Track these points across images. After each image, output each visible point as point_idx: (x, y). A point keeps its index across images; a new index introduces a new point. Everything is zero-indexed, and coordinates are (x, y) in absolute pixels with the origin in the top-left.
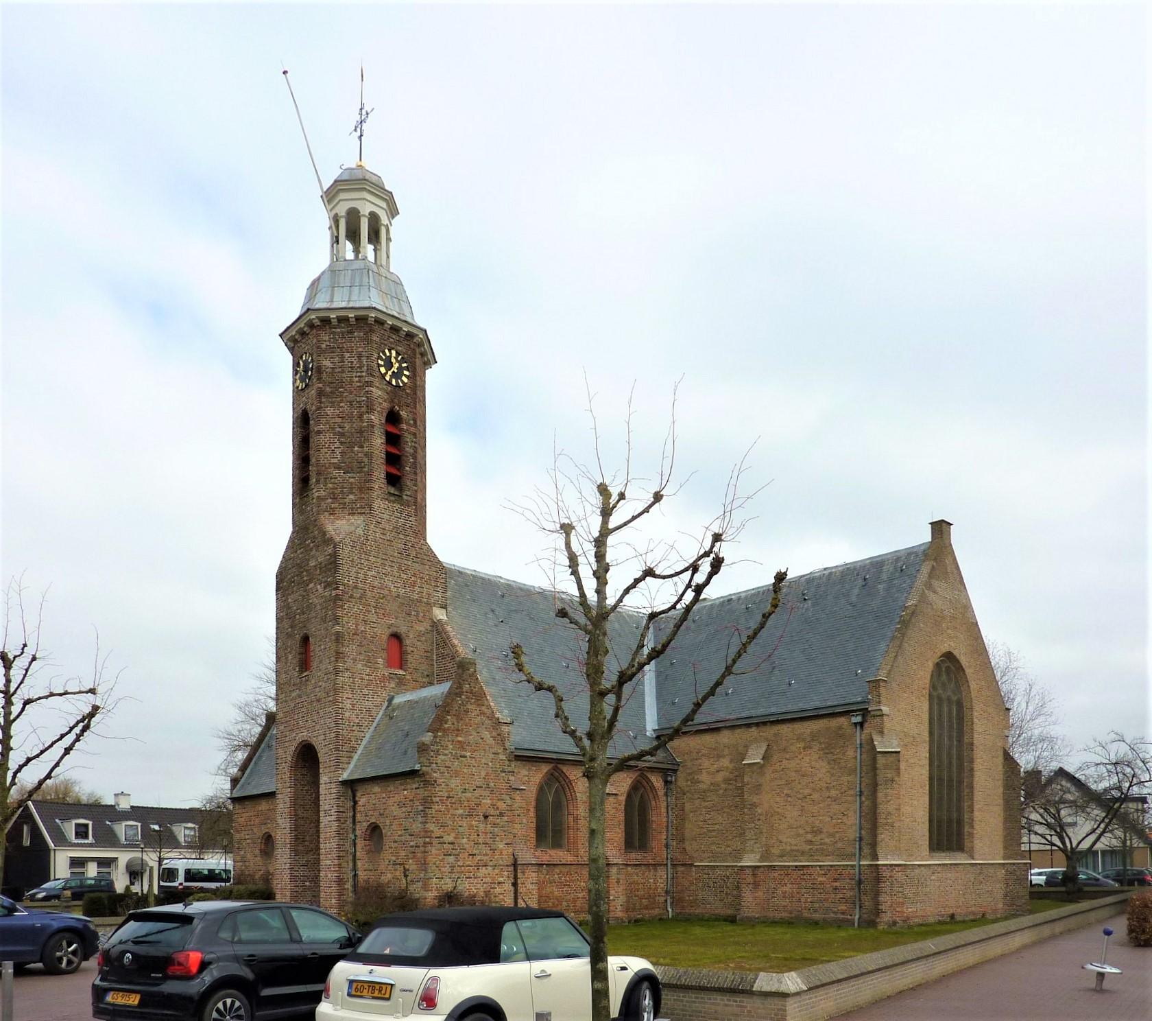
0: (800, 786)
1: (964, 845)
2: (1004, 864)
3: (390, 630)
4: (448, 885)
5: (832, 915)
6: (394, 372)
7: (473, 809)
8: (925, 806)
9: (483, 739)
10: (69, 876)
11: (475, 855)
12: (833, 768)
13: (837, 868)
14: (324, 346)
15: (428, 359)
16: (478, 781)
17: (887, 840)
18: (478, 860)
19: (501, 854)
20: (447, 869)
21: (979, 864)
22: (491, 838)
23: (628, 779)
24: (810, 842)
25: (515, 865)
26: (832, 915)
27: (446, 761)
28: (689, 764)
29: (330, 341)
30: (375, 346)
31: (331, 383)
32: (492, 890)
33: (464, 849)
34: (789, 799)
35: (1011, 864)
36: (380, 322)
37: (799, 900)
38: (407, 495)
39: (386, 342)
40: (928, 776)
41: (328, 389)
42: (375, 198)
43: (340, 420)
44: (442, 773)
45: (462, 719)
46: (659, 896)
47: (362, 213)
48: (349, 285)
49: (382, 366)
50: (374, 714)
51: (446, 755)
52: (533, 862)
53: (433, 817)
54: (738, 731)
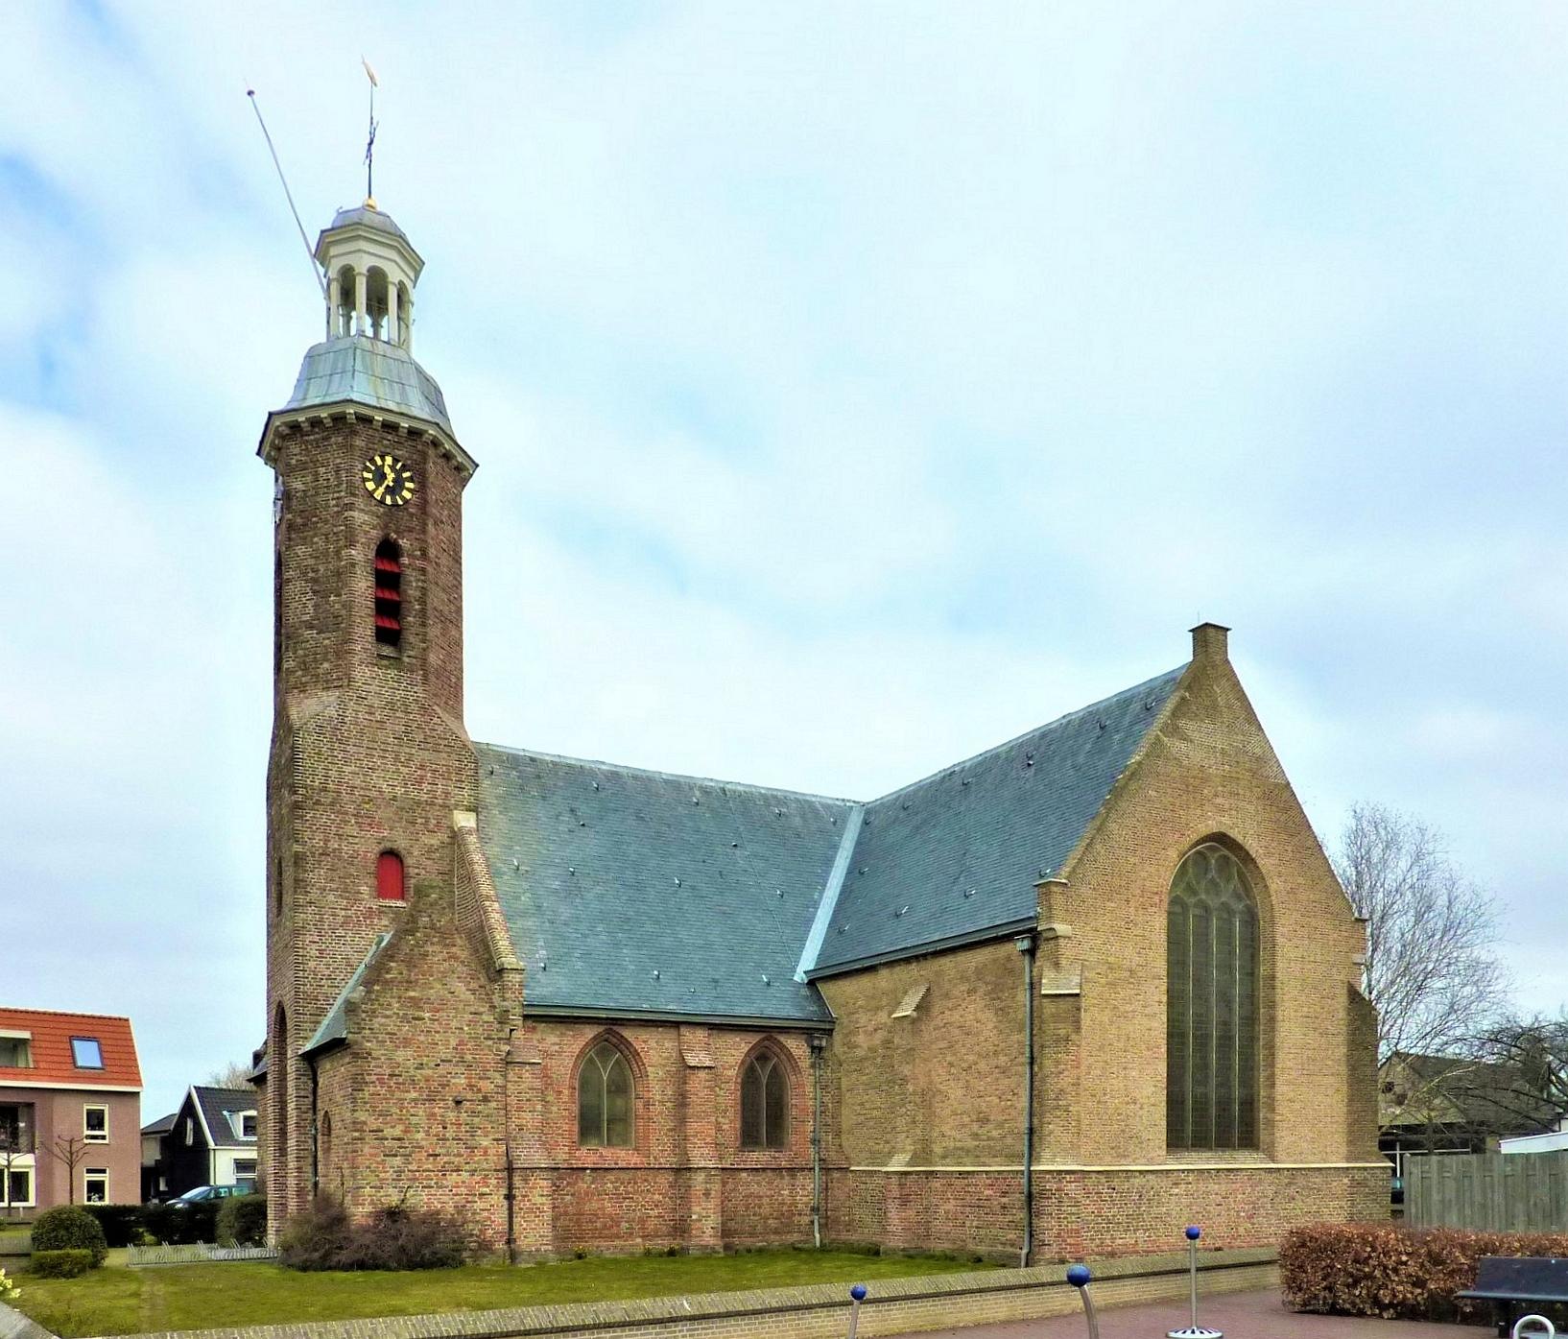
0: (964, 1051)
1: (1259, 1138)
2: (1348, 1168)
3: (382, 846)
4: (393, 1198)
5: (1000, 1248)
6: (388, 486)
7: (437, 1092)
10: (234, 1182)
12: (1000, 1022)
13: (1005, 1175)
14: (294, 462)
15: (460, 469)
16: (444, 1052)
17: (1057, 1133)
18: (445, 1163)
19: (486, 1153)
20: (390, 1174)
21: (1288, 1169)
22: (467, 1132)
23: (743, 1045)
24: (975, 1136)
25: (510, 1169)
26: (1000, 1248)
28: (845, 1021)
29: (301, 454)
30: (358, 453)
31: (302, 511)
32: (468, 1205)
33: (419, 1147)
34: (953, 1070)
35: (1359, 1168)
36: (367, 420)
37: (963, 1225)
38: (409, 657)
39: (376, 446)
40: (1165, 1031)
41: (299, 520)
43: (311, 562)
44: (381, 1041)
46: (800, 1215)
47: (357, 271)
48: (329, 372)
49: (369, 480)
50: (354, 961)
51: (387, 1017)
52: (543, 1166)
53: (365, 1103)
54: (897, 969)
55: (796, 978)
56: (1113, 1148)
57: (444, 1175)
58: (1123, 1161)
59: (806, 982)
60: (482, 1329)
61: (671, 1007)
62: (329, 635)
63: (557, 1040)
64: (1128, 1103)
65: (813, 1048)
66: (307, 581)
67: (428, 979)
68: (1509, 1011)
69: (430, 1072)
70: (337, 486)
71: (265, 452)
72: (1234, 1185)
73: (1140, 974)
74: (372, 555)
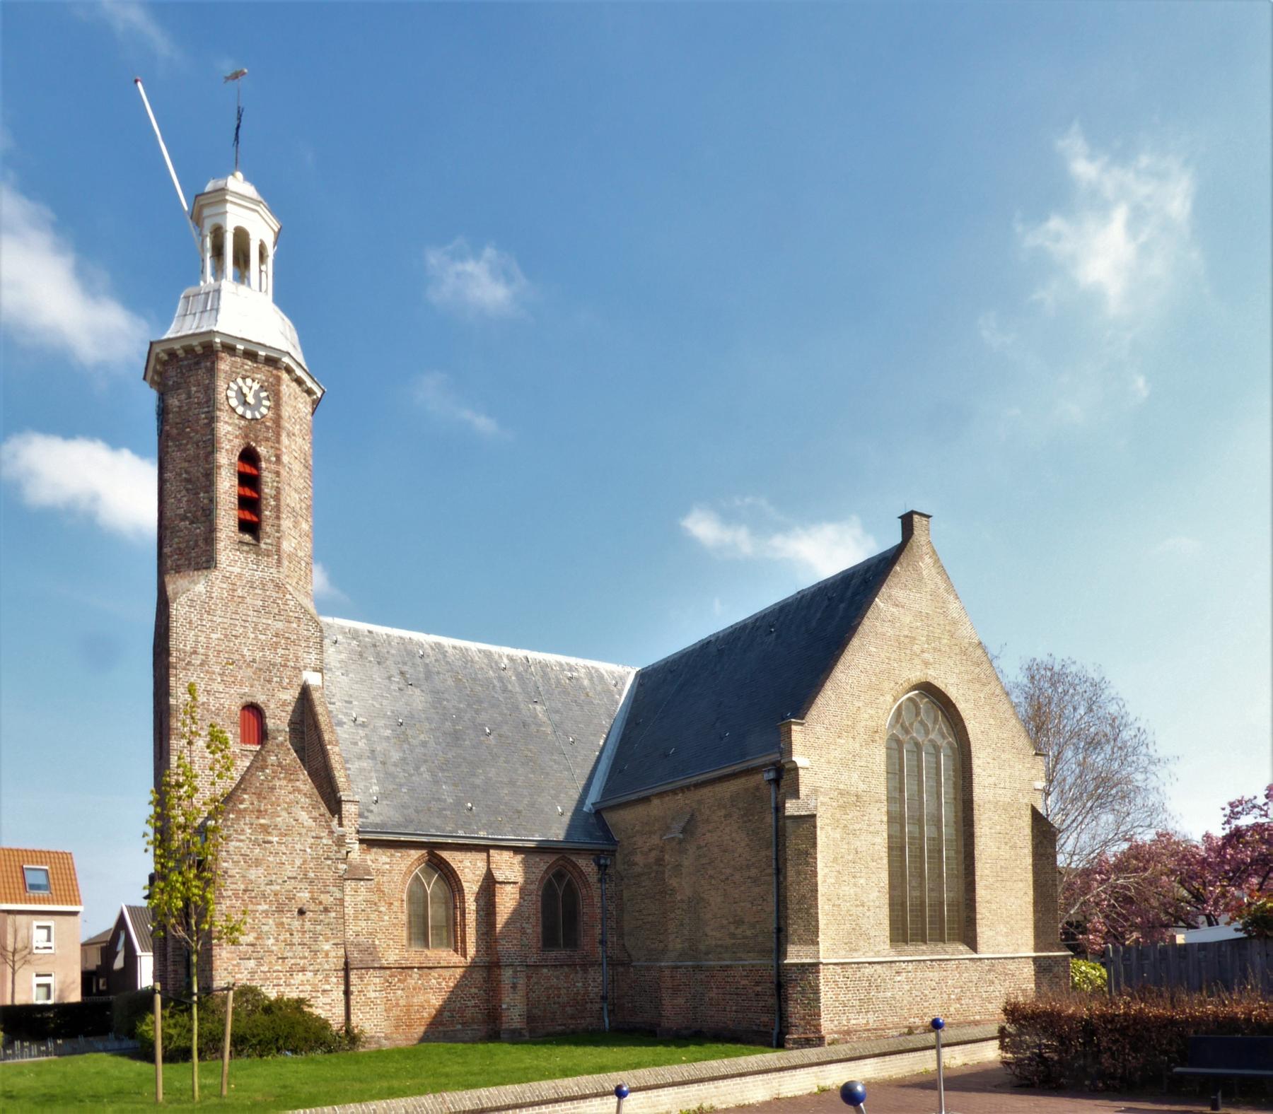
0: (722, 865)
3: (243, 700)
8: (882, 884)
9: (297, 820)
11: (287, 958)
14: (171, 383)
16: (289, 871)
19: (327, 955)
21: (988, 959)
22: (310, 938)
24: (733, 936)
25: (347, 969)
27: (242, 848)
34: (713, 882)
39: (238, 370)
42: (252, 203)
43: (186, 465)
45: (265, 798)
55: (585, 809)
56: (846, 944)
57: (291, 975)
58: (855, 954)
59: (593, 812)
60: (469, 1106)
61: (482, 834)
62: (199, 525)
63: (388, 860)
64: (857, 906)
65: (599, 866)
66: (181, 481)
67: (276, 809)
68: (1171, 826)
69: (278, 888)
70: (207, 402)
71: (149, 377)
72: (945, 973)
73: (865, 799)
74: (235, 459)
